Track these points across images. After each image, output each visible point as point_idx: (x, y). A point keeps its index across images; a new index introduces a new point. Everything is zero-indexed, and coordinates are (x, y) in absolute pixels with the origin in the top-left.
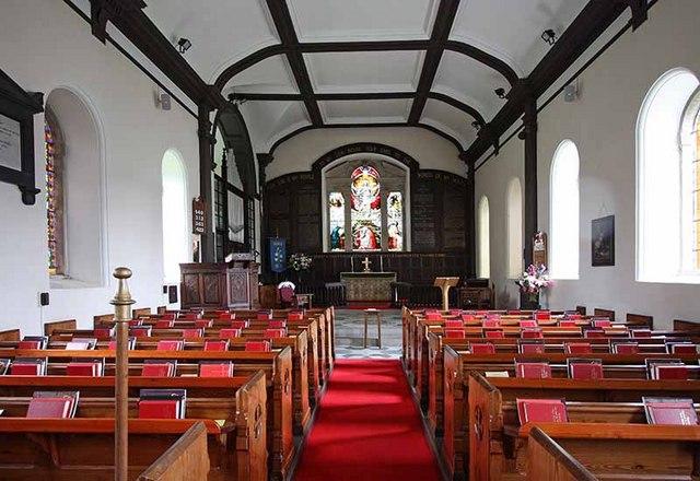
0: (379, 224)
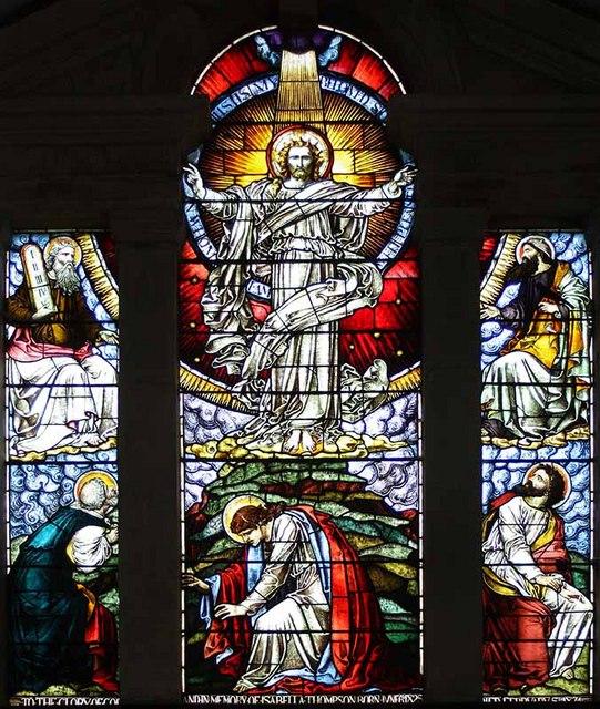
0: (407, 494)
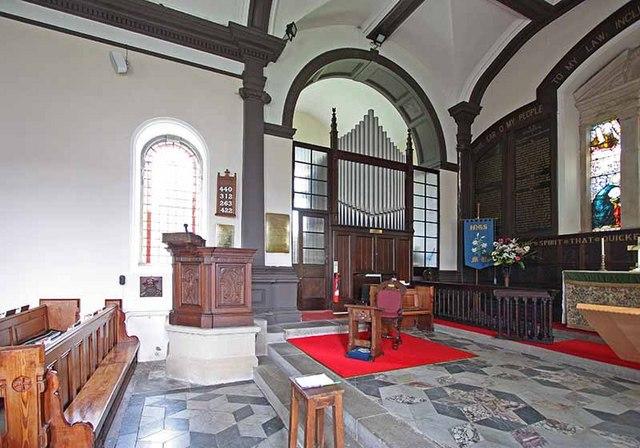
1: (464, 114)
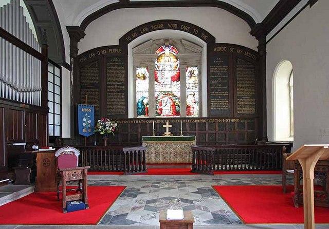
0: (178, 95)
1: (77, 33)
